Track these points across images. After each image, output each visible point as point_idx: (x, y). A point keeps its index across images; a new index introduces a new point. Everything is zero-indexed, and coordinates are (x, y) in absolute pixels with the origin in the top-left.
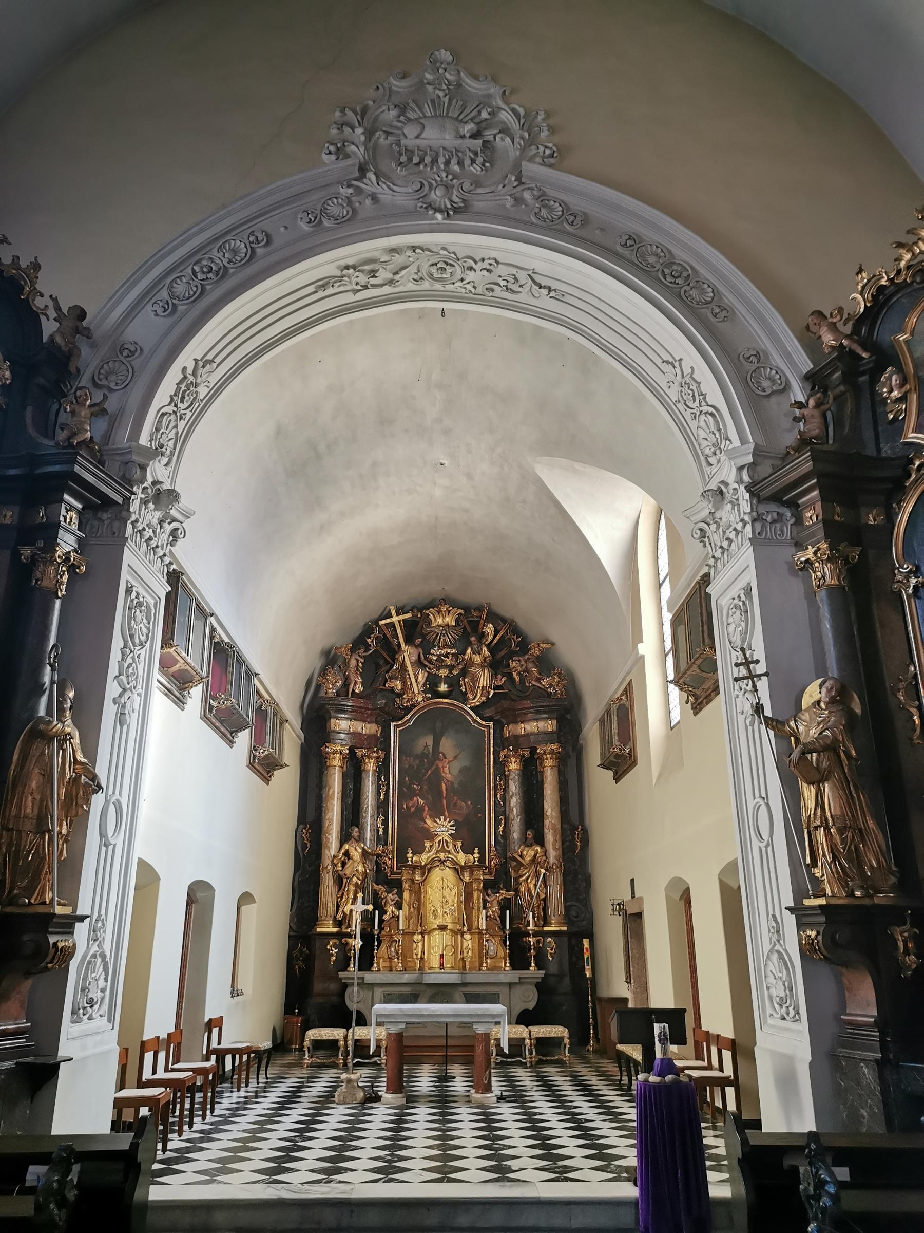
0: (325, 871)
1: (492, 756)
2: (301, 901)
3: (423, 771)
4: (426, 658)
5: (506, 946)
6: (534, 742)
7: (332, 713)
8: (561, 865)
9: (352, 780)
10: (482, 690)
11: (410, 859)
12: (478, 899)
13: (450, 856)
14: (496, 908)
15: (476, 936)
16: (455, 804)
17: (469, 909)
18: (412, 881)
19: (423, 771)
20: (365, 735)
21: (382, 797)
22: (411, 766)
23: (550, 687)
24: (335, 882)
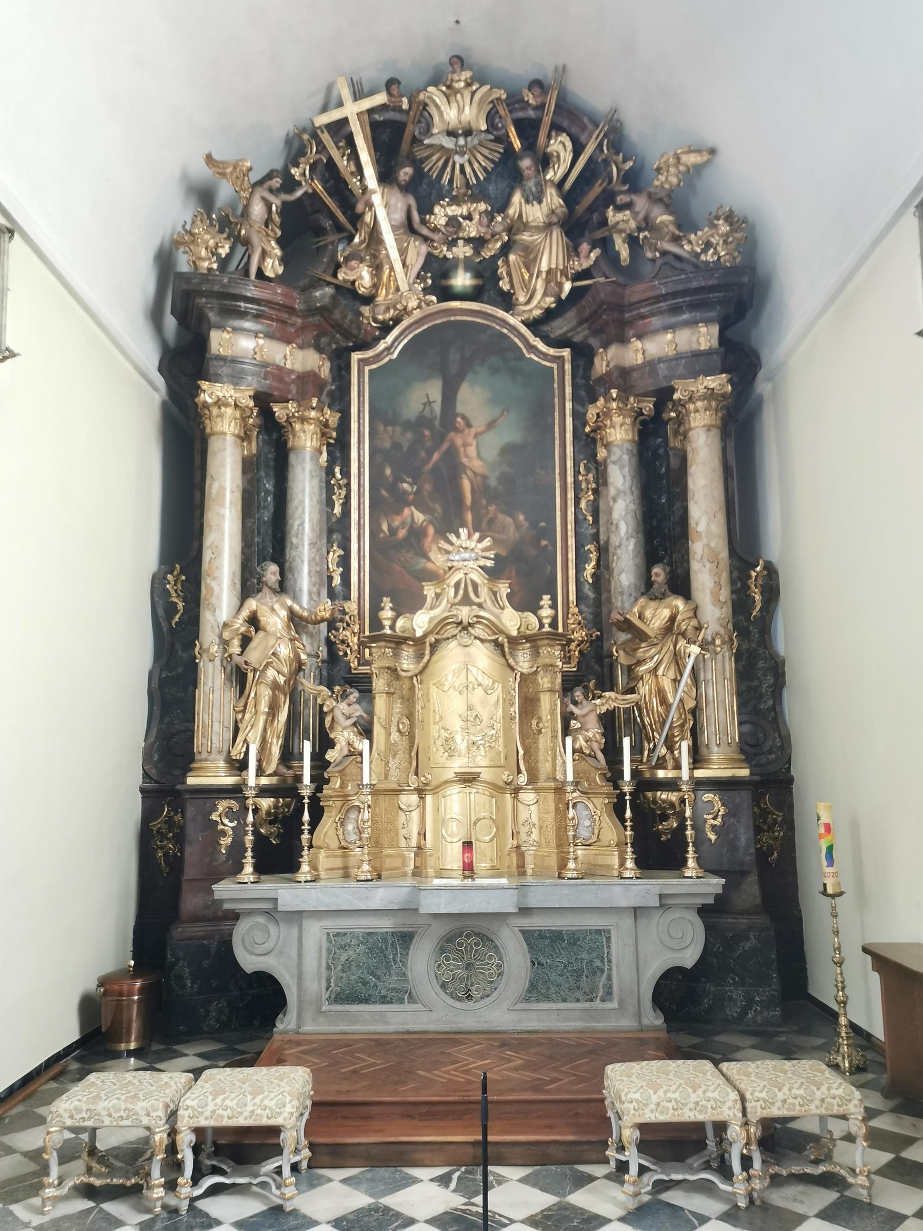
0: (205, 655)
1: (569, 421)
2: (166, 720)
3: (423, 454)
4: (424, 222)
5: (623, 820)
6: (665, 377)
7: (213, 317)
8: (731, 640)
9: (272, 473)
10: (547, 281)
11: (387, 623)
12: (552, 713)
13: (482, 613)
14: (594, 731)
15: (551, 796)
16: (491, 522)
17: (529, 736)
18: (393, 671)
19: (423, 454)
20: (292, 371)
21: (337, 510)
22: (396, 446)
23: (704, 251)
24: (228, 679)
